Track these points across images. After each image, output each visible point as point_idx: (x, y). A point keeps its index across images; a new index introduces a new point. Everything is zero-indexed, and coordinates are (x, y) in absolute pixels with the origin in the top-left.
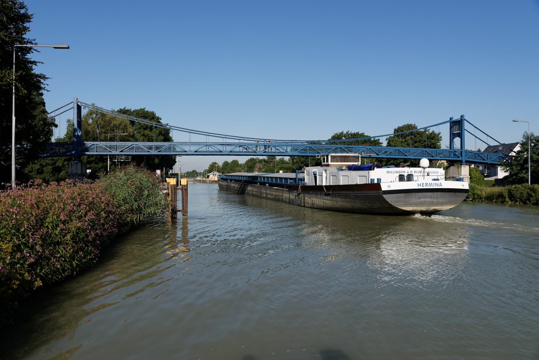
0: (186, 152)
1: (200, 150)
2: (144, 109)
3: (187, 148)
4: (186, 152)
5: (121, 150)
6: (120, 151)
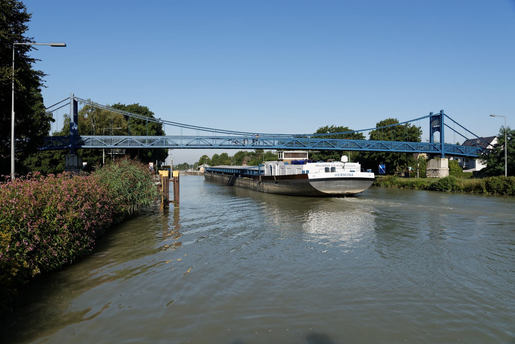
0: (177, 145)
2: (137, 105)
3: (178, 142)
4: (177, 145)
5: (116, 143)
6: (115, 144)
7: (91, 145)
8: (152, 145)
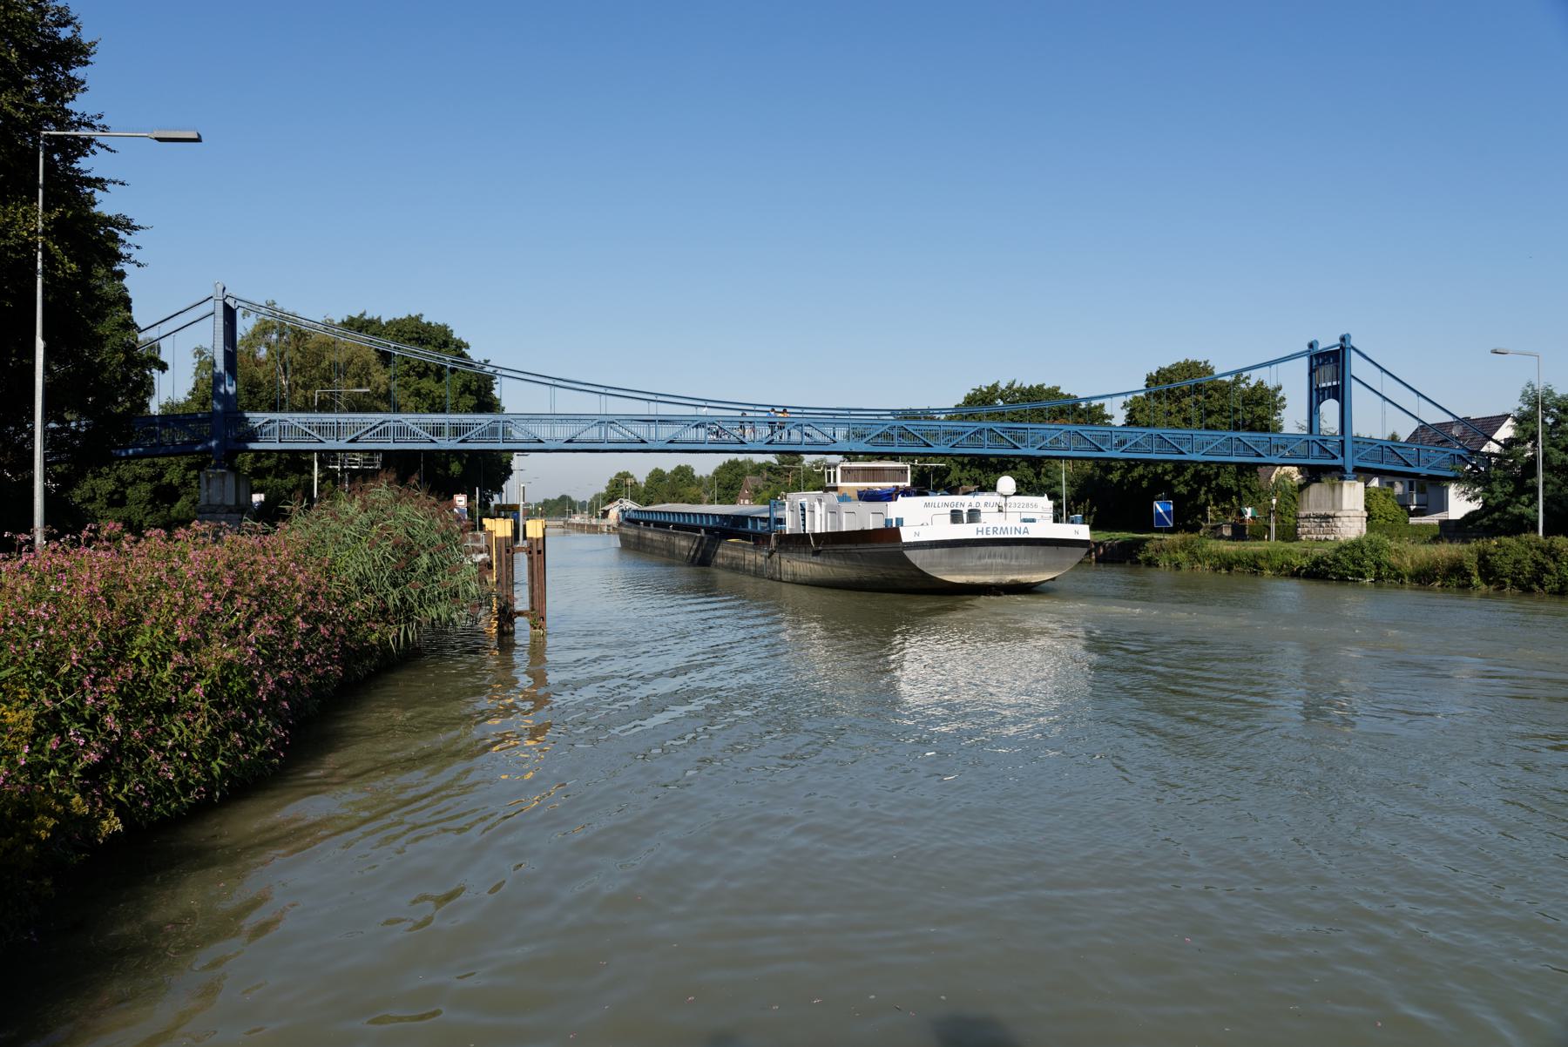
0: (540, 441)
1: (583, 437)
3: (543, 432)
4: (540, 441)
5: (353, 436)
6: (349, 438)
7: (277, 440)
8: (463, 441)
